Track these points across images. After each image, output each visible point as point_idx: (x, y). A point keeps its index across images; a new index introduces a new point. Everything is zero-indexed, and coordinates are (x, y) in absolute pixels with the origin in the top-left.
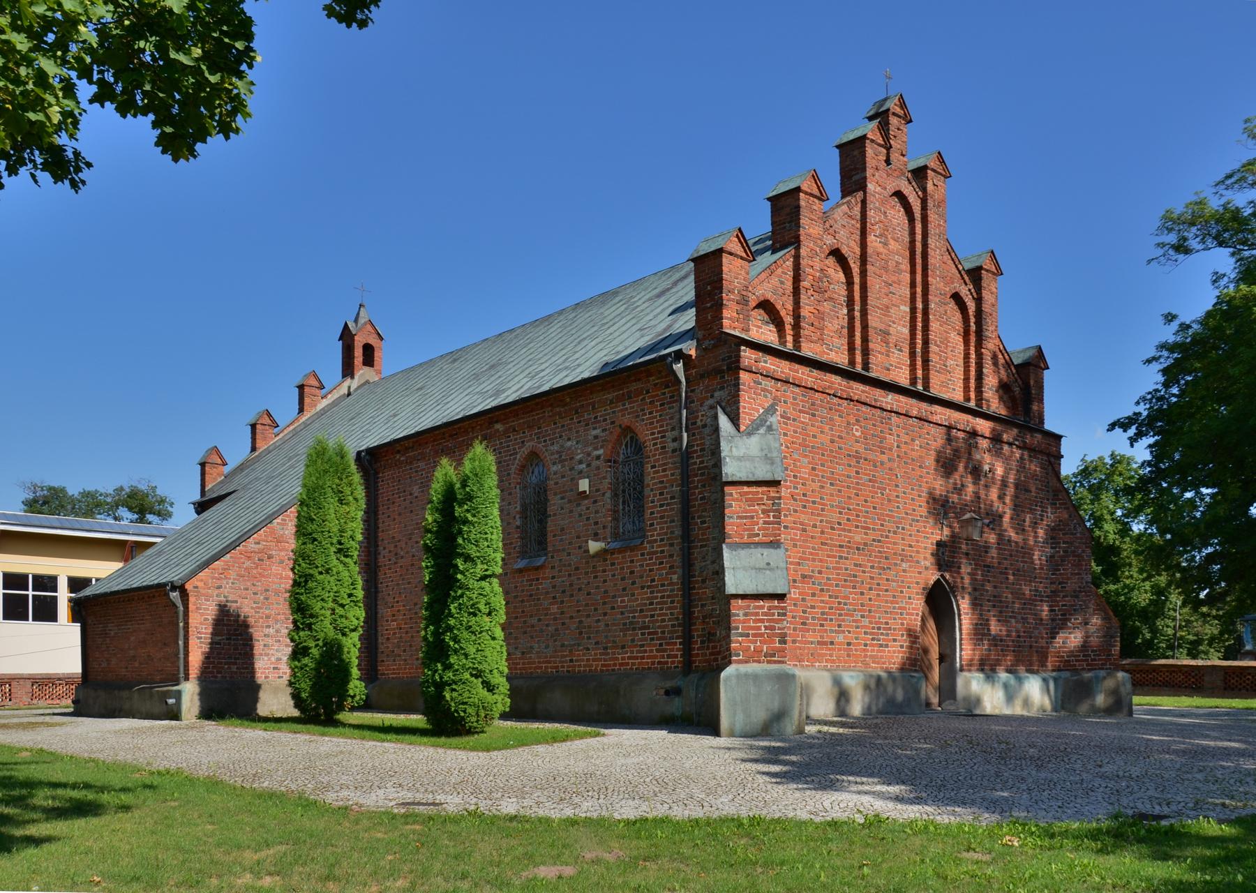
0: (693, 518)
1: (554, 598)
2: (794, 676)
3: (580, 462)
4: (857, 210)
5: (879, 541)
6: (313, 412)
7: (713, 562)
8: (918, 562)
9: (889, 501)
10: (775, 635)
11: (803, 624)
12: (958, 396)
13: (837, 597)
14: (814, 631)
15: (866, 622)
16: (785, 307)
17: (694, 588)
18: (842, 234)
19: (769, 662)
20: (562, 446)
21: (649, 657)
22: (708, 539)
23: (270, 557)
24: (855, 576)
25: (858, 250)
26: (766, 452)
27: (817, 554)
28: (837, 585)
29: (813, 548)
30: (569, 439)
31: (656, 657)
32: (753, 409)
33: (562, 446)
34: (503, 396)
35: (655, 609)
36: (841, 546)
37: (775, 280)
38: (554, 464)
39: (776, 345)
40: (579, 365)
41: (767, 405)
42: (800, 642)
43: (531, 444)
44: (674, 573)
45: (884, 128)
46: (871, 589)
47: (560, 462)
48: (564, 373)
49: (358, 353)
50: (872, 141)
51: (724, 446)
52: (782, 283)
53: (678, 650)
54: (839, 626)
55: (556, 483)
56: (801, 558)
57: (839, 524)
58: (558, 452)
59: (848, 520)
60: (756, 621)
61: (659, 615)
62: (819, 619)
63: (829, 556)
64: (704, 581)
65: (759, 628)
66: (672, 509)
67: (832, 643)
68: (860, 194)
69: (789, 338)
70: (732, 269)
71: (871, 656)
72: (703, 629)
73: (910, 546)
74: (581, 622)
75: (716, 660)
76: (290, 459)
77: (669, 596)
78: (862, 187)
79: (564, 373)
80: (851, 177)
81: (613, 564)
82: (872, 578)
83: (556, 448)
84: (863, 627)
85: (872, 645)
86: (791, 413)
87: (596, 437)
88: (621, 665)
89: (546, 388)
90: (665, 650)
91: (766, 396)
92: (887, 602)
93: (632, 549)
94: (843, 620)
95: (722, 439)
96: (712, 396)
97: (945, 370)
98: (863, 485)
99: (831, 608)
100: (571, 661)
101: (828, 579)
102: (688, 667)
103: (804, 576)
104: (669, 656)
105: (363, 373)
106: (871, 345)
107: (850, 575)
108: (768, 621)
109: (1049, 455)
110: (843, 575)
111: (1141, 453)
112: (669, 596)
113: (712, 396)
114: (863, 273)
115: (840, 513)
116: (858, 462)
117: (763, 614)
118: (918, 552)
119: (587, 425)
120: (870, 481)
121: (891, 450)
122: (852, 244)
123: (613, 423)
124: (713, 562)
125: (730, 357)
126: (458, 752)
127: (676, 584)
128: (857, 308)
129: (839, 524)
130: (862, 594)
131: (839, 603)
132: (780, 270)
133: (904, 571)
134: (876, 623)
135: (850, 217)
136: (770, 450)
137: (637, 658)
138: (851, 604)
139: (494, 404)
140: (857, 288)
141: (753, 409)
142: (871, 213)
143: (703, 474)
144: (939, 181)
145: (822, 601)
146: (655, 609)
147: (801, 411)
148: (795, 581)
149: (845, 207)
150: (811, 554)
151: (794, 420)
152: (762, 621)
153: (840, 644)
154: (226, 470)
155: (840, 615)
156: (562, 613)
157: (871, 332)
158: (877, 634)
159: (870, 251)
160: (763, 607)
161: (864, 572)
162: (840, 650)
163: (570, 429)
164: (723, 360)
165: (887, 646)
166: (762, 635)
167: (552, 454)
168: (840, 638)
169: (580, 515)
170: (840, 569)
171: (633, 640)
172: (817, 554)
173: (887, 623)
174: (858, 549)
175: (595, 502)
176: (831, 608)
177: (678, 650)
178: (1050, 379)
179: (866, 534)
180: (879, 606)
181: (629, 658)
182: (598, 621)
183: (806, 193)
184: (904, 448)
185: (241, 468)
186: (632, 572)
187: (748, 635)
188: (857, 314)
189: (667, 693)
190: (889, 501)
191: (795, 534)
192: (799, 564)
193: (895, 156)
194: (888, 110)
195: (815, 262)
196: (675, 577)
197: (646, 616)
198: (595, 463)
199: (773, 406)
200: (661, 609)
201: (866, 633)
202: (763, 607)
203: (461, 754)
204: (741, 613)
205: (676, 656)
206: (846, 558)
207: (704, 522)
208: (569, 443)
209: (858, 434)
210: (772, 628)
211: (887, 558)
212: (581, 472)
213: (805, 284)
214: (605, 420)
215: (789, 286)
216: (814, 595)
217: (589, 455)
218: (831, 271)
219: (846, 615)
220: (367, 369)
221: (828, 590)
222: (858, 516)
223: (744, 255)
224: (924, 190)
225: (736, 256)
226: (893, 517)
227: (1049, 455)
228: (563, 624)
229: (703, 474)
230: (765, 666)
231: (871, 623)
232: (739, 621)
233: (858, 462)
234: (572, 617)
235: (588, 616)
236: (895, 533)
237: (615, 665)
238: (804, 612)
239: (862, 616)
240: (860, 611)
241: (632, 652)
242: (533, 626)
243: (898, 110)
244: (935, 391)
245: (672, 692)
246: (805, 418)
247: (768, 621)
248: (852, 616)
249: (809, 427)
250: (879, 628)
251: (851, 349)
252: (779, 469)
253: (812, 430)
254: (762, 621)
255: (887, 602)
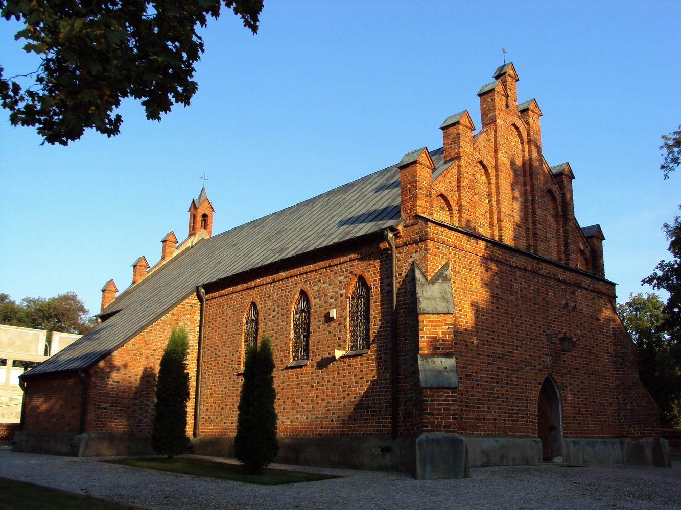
0: (399, 337)
1: (312, 386)
2: (462, 441)
3: (331, 298)
4: (492, 135)
5: (512, 353)
6: (170, 258)
7: (412, 366)
8: (535, 366)
9: (517, 326)
10: (451, 414)
11: (467, 406)
12: (554, 257)
13: (487, 389)
14: (473, 411)
15: (504, 405)
16: (453, 198)
17: (399, 382)
18: (484, 151)
19: (446, 432)
20: (320, 287)
21: (371, 427)
22: (408, 351)
23: (141, 354)
24: (498, 375)
25: (493, 162)
26: (443, 294)
27: (475, 361)
28: (487, 381)
29: (472, 357)
30: (324, 283)
31: (374, 427)
32: (436, 266)
33: (320, 287)
34: (286, 253)
35: (375, 396)
36: (489, 356)
37: (446, 181)
38: (315, 298)
39: (448, 223)
40: (332, 234)
41: (444, 263)
42: (465, 418)
43: (301, 285)
44: (388, 372)
45: (504, 83)
46: (507, 384)
47: (319, 297)
48: (323, 239)
49: (199, 219)
50: (498, 92)
51: (418, 289)
52: (450, 183)
53: (389, 422)
54: (489, 408)
55: (316, 311)
56: (465, 364)
57: (488, 341)
58: (317, 291)
59: (493, 339)
60: (438, 405)
61: (378, 400)
62: (476, 404)
63: (482, 362)
64: (406, 378)
65: (440, 410)
66: (387, 331)
67: (484, 419)
68: (493, 126)
69: (456, 219)
70: (423, 173)
71: (509, 428)
72: (405, 410)
73: (530, 356)
74: (328, 403)
75: (413, 429)
76: (155, 290)
77: (384, 388)
78: (494, 121)
79: (323, 239)
80: (487, 115)
81: (349, 366)
82: (508, 377)
83: (316, 288)
84: (504, 408)
85: (508, 420)
86: (458, 268)
87: (341, 282)
88: (353, 431)
89: (311, 249)
90: (381, 423)
91: (442, 257)
92: (517, 392)
93: (361, 355)
94: (491, 404)
95: (417, 285)
96: (411, 257)
97: (546, 240)
98: (501, 316)
99: (483, 396)
100: (322, 428)
101: (481, 377)
102: (395, 434)
103: (467, 375)
104: (384, 427)
105: (202, 234)
106: (503, 224)
107: (494, 375)
108: (446, 405)
109: (608, 296)
110: (491, 375)
111: (664, 296)
112: (384, 388)
113: (411, 257)
114: (497, 176)
115: (488, 334)
116: (498, 301)
117: (443, 401)
118: (535, 360)
119: (336, 273)
120: (505, 313)
121: (516, 292)
122: (490, 158)
123: (351, 273)
124: (412, 366)
125: (421, 232)
126: (252, 485)
127: (389, 379)
128: (494, 199)
129: (488, 341)
130: (502, 387)
131: (489, 393)
132: (449, 175)
133: (527, 372)
134: (511, 406)
135: (487, 140)
136: (446, 293)
137: (363, 427)
138: (496, 394)
139: (280, 258)
140: (493, 186)
141: (436, 266)
142: (499, 138)
143: (405, 308)
144: (535, 117)
145: (478, 392)
146: (375, 396)
147: (463, 267)
148: (461, 379)
149: (484, 134)
150: (471, 361)
151: (460, 273)
152: (442, 405)
153: (489, 419)
154: (117, 295)
155: (489, 401)
156: (317, 396)
157: (503, 215)
158: (512, 413)
159: (500, 162)
160: (442, 396)
161: (503, 373)
162: (489, 423)
163: (325, 276)
164: (417, 233)
165: (518, 421)
166: (442, 414)
167: (314, 292)
168: (489, 416)
169: (330, 333)
170: (489, 370)
171: (361, 416)
172: (475, 361)
173: (517, 406)
174: (499, 358)
175: (339, 324)
176: (483, 396)
177: (389, 422)
178: (577, 186)
179: (503, 348)
180: (513, 395)
181: (358, 427)
182: (340, 402)
183: (463, 125)
184: (524, 291)
185: (126, 294)
186: (361, 371)
187: (433, 414)
188: (494, 203)
189: (382, 450)
190: (517, 326)
191: (461, 348)
192: (463, 368)
193: (510, 101)
194: (506, 73)
195: (470, 170)
196: (388, 375)
197: (370, 400)
198: (340, 299)
199: (447, 263)
200: (379, 396)
201: (505, 413)
202: (442, 396)
203: (255, 487)
204: (429, 399)
205: (388, 427)
206: (492, 364)
207: (406, 339)
208: (325, 285)
209: (497, 282)
210: (449, 410)
211: (516, 364)
212: (331, 304)
213: (463, 184)
214: (346, 271)
215: (455, 184)
216: (473, 388)
217: (336, 293)
218: (478, 175)
219: (493, 401)
220: (203, 230)
221: (482, 385)
222: (498, 336)
223: (429, 165)
224: (527, 123)
225: (425, 165)
226: (519, 337)
227: (608, 296)
228: (318, 404)
229: (405, 308)
230: (444, 434)
231: (508, 406)
232: (428, 405)
233: (498, 301)
234: (322, 400)
235: (333, 399)
236: (521, 347)
237: (349, 431)
238: (467, 399)
239: (503, 402)
240: (501, 398)
241: (360, 423)
242: (298, 405)
243: (511, 72)
244: (542, 254)
245: (386, 450)
246: (466, 272)
247: (446, 405)
248: (496, 401)
249: (468, 278)
250: (513, 410)
251: (492, 226)
252: (452, 306)
253: (469, 280)
254: (442, 405)
255: (517, 392)
